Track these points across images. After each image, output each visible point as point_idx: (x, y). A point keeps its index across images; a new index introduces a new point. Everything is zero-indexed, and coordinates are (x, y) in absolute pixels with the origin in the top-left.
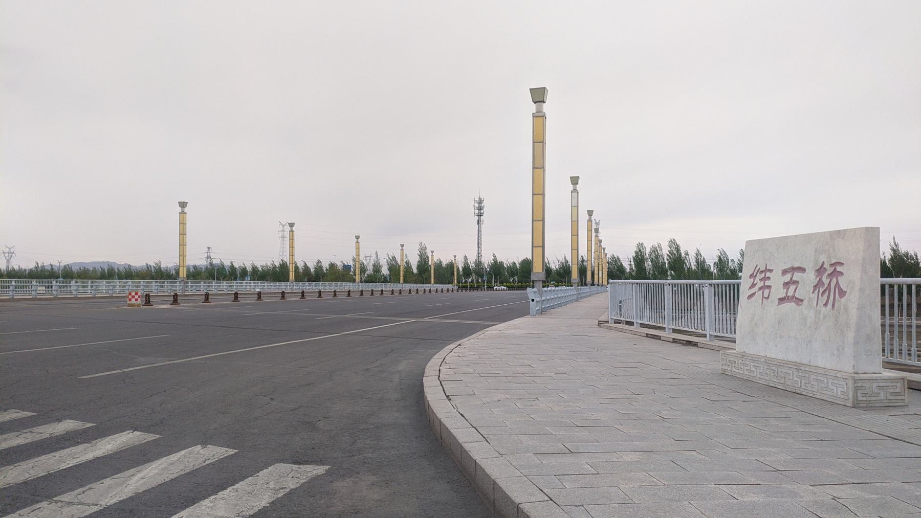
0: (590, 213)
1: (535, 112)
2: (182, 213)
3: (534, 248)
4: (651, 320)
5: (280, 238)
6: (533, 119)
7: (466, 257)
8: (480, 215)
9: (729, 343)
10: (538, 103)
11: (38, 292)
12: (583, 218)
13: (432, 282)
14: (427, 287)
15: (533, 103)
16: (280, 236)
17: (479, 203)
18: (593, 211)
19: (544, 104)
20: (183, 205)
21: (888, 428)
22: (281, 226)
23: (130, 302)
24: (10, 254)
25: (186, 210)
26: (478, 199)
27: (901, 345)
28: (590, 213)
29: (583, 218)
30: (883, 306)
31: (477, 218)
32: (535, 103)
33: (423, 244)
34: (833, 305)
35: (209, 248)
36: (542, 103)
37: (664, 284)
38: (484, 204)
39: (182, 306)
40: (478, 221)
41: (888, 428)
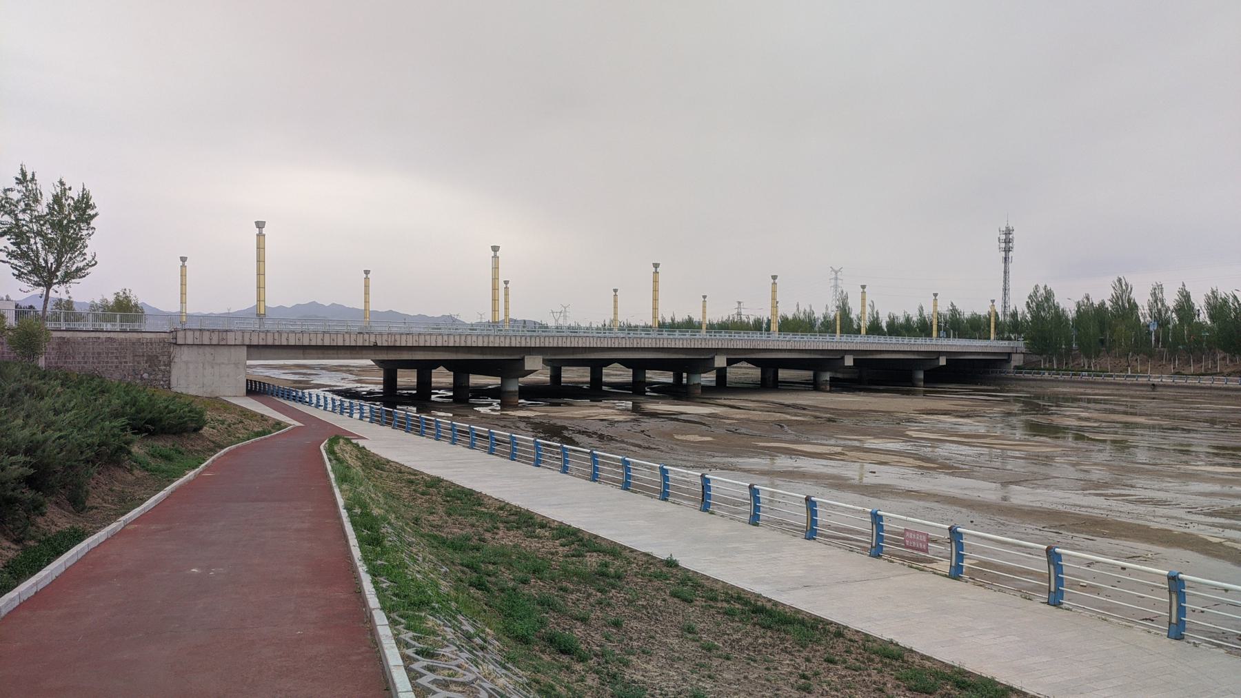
5: (833, 288)
7: (922, 308)
8: (1007, 250)
9: (593, 345)
13: (992, 336)
16: (833, 285)
17: (1006, 234)
21: (1123, 458)
22: (833, 273)
24: (564, 313)
26: (1004, 229)
28: (506, 282)
29: (502, 286)
31: (1003, 253)
33: (845, 293)
34: (48, 300)
35: (739, 303)
38: (1014, 235)
40: (1005, 258)
41: (1123, 458)
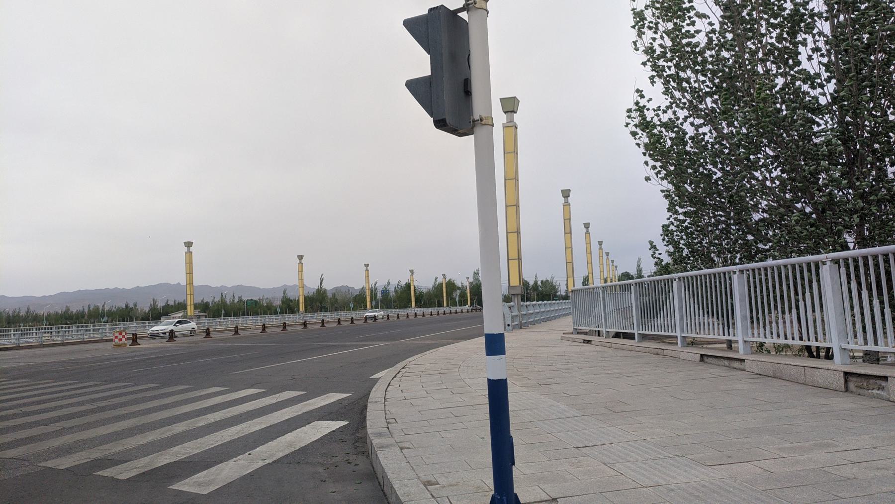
0: (600, 243)
1: (506, 122)
2: (189, 253)
3: (510, 261)
4: (647, 328)
6: (503, 129)
10: (509, 113)
11: (43, 339)
12: (595, 246)
14: (441, 310)
15: (503, 113)
18: (602, 242)
19: (515, 114)
20: (189, 245)
23: (121, 342)
25: (191, 249)
27: (704, 320)
28: (600, 243)
29: (595, 246)
30: (752, 318)
32: (505, 112)
36: (513, 113)
37: (630, 284)
39: (144, 345)
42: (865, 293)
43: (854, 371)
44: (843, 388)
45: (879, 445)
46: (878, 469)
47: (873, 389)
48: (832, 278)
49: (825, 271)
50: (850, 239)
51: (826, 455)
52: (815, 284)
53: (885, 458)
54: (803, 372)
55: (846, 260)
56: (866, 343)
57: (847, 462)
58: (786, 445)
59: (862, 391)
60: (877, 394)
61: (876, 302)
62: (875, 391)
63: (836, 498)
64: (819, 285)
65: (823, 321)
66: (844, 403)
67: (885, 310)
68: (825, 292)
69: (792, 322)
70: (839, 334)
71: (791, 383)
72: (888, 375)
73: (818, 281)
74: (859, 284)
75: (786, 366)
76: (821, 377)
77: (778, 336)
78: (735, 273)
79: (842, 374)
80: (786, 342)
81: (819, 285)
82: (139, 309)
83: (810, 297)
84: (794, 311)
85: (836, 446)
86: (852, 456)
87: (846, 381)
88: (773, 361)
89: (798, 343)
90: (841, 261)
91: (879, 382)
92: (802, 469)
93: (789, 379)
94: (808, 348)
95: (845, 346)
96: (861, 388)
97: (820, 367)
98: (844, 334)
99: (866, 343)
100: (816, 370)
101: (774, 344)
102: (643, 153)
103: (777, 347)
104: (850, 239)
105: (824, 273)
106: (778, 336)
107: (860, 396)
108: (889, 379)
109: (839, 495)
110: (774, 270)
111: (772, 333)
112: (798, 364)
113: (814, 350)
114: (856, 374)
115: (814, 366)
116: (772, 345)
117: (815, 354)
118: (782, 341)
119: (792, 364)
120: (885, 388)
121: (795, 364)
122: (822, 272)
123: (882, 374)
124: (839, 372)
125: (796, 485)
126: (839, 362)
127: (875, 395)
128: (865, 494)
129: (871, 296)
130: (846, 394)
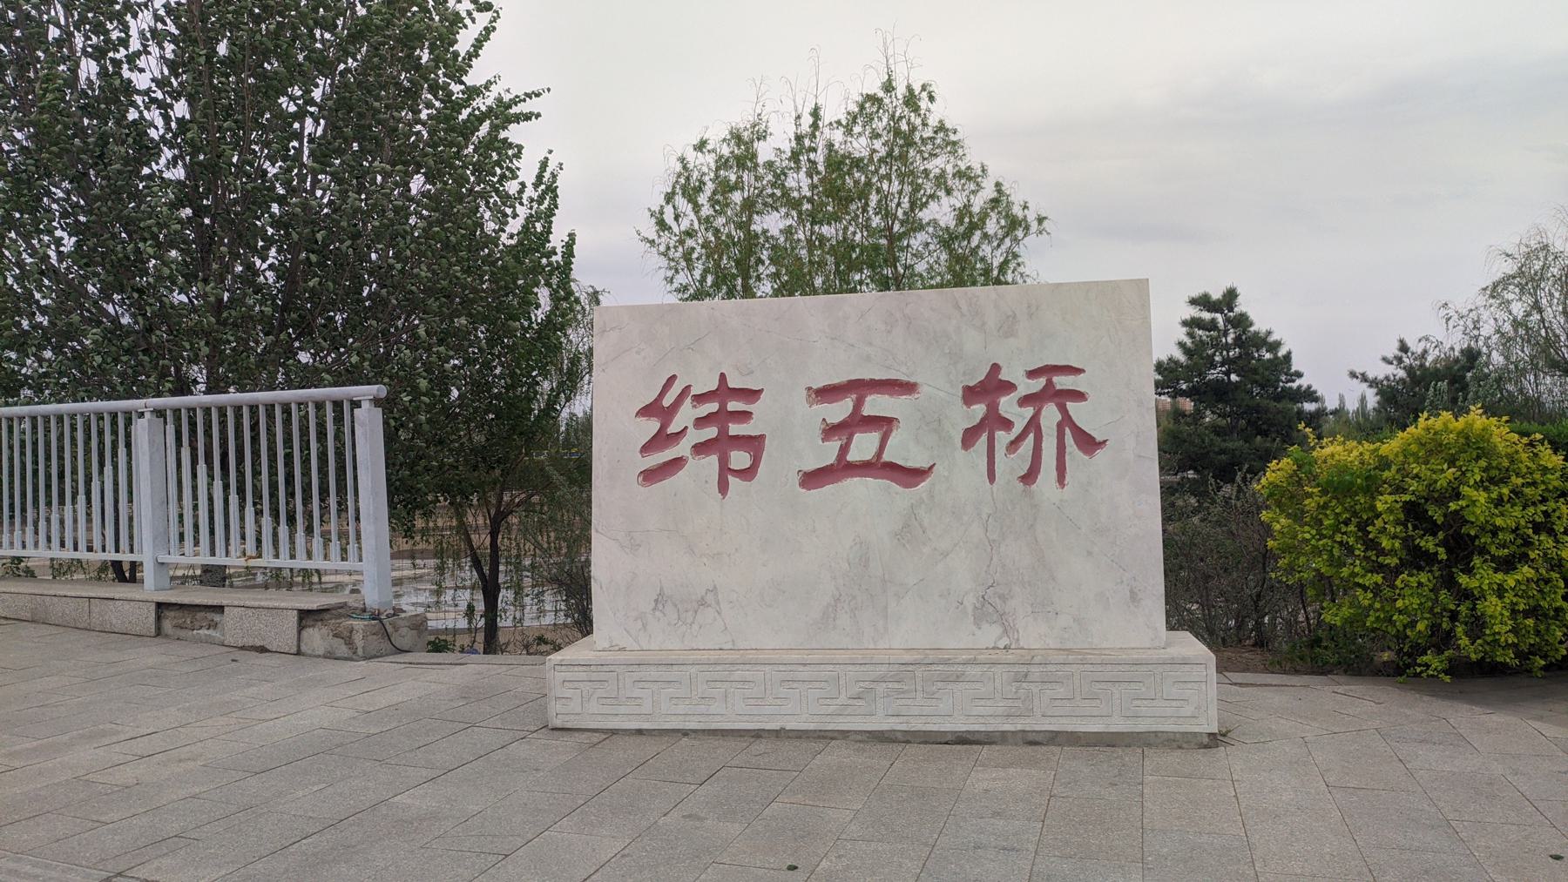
42: (202, 468)
43: (173, 600)
44: (153, 630)
45: (190, 721)
46: (180, 761)
47: (201, 627)
48: (151, 442)
49: (141, 428)
50: (198, 373)
51: (97, 751)
52: (122, 451)
53: (195, 740)
54: (86, 608)
55: (177, 412)
56: (213, 553)
57: (130, 758)
58: (27, 745)
59: (182, 633)
60: (206, 635)
61: (218, 484)
62: (204, 632)
63: (96, 824)
64: (129, 454)
65: (131, 519)
66: (151, 656)
67: (231, 498)
68: (138, 466)
69: (75, 521)
70: (155, 538)
71: (61, 630)
72: (225, 602)
73: (128, 445)
74: (194, 450)
75: (56, 599)
76: (114, 616)
77: (62, 545)
78: (356, 404)
79: (153, 607)
80: (77, 555)
81: (129, 454)
82: (527, 169)
83: (111, 473)
84: (81, 498)
85: (118, 733)
86: (141, 746)
87: (159, 618)
88: (33, 591)
89: (98, 556)
90: (168, 412)
91: (210, 616)
92: (45, 784)
93: (60, 621)
94: (117, 565)
95: (163, 558)
96: (182, 628)
97: (117, 596)
98: (162, 539)
99: (213, 553)
100: (111, 603)
101: (52, 560)
102: (536, 118)
103: (56, 566)
104: (198, 373)
105: (138, 433)
106: (62, 545)
107: (178, 642)
108: (226, 609)
109: (103, 819)
110: (290, 414)
111: (49, 540)
112: (78, 594)
113: (126, 567)
114: (176, 604)
115: (107, 595)
116: (48, 563)
117: (127, 575)
118: (68, 554)
119: (69, 594)
120: (219, 625)
121: (73, 594)
122: (136, 430)
123: (215, 602)
124: (148, 604)
125: (28, 815)
126: (151, 587)
127: (203, 637)
128: (148, 808)
129: (211, 477)
130: (156, 640)
